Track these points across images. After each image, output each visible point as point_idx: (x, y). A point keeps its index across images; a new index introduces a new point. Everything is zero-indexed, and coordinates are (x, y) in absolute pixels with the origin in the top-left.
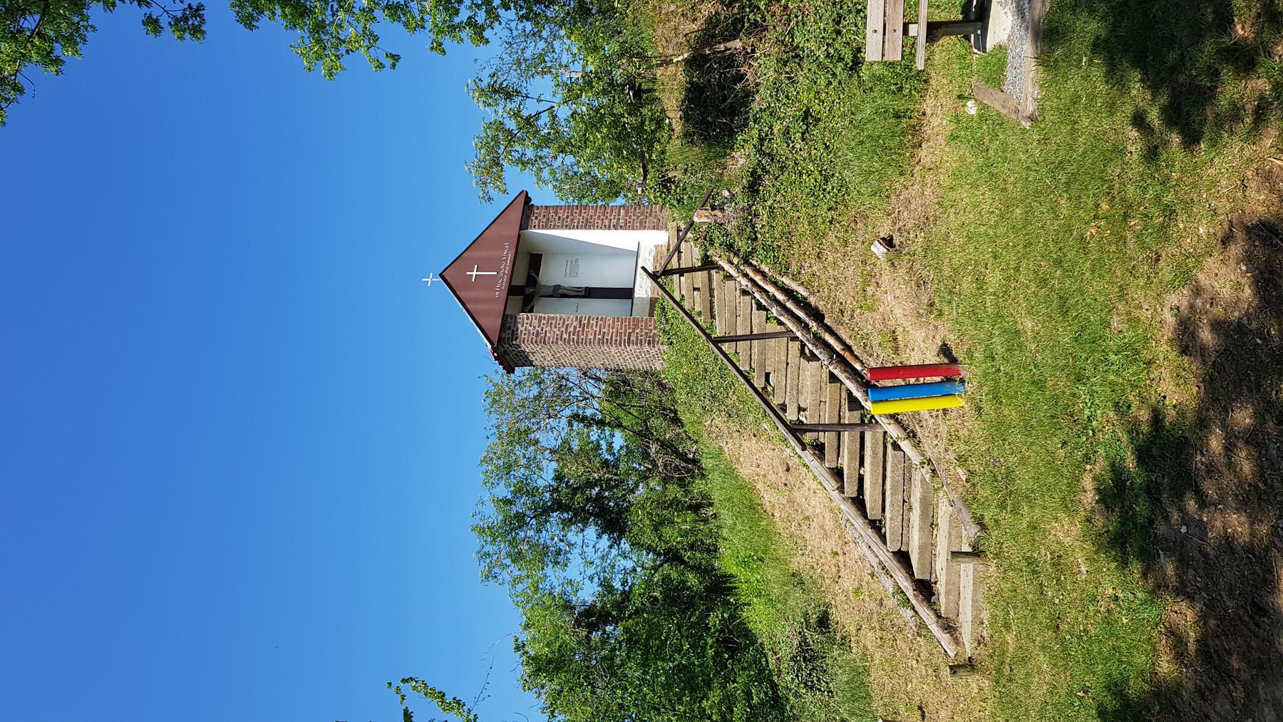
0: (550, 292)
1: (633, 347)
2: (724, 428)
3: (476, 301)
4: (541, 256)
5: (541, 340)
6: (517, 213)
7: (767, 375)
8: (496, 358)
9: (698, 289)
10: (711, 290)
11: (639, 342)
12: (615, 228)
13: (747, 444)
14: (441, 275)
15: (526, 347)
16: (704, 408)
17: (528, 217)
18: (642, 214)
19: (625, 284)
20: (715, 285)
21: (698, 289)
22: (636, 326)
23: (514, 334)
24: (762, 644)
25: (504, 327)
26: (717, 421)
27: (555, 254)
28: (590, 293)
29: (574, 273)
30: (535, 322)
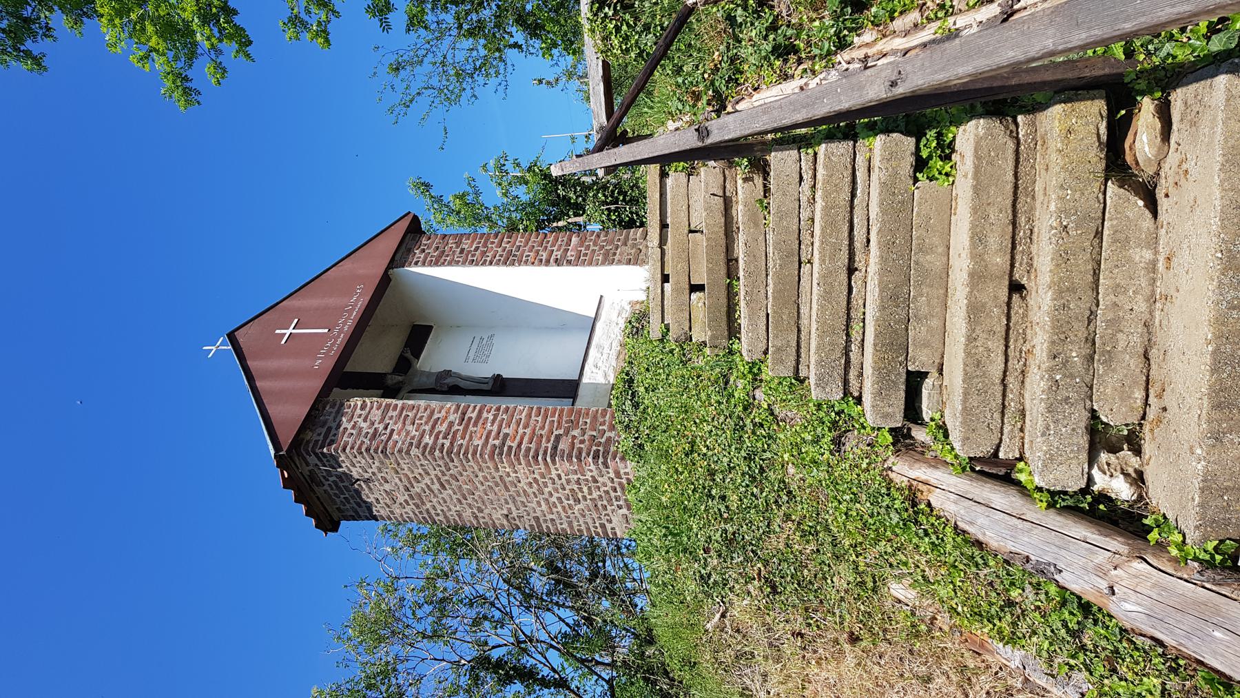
0: (430, 383)
1: (563, 467)
2: (757, 633)
5: (379, 447)
6: (389, 244)
7: (914, 382)
8: (287, 484)
9: (698, 288)
10: (731, 294)
12: (558, 262)
13: (829, 673)
14: (232, 337)
15: (353, 466)
16: (704, 579)
19: (565, 372)
20: (739, 212)
21: (698, 288)
22: (574, 424)
23: (331, 435)
25: (312, 419)
26: (740, 608)
27: (455, 327)
28: (500, 387)
29: (483, 355)
30: (376, 414)
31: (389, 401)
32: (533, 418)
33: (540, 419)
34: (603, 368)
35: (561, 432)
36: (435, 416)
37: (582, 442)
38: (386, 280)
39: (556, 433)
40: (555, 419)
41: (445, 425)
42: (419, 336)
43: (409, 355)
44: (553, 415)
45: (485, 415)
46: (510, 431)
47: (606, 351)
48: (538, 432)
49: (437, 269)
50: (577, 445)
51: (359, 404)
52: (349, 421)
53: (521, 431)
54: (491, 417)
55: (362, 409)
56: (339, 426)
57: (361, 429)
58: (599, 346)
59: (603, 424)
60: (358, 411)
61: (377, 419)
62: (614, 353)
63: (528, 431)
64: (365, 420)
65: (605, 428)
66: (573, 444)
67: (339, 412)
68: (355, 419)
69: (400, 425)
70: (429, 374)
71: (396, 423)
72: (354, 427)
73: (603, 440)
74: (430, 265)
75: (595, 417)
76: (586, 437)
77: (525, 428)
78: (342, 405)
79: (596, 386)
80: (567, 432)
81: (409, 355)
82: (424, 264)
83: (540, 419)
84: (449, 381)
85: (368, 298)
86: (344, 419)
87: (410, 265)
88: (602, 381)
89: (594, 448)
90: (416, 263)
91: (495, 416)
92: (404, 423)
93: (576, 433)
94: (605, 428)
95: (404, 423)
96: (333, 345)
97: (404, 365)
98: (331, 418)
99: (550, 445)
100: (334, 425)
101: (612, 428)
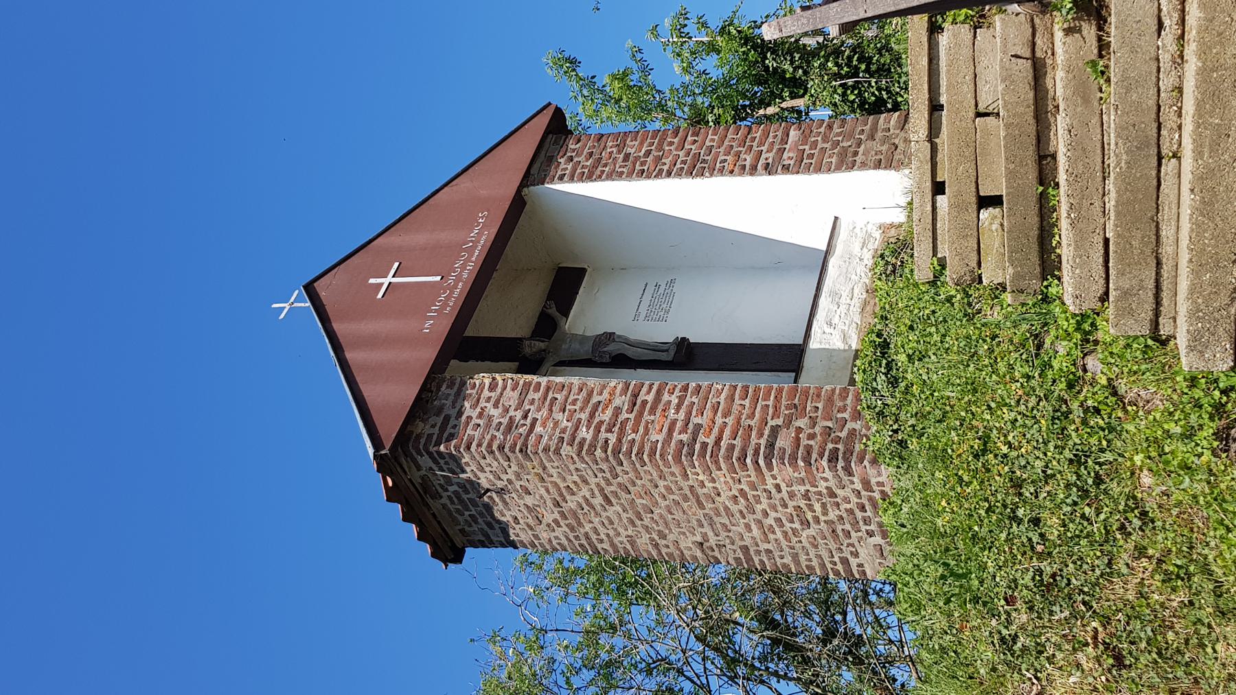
0: (585, 351)
1: (783, 473)
3: (371, 342)
4: (581, 272)
5: (517, 444)
9: (995, 201)
11: (802, 455)
12: (769, 170)
15: (481, 470)
16: (1007, 643)
17: (551, 160)
18: (851, 135)
19: (782, 332)
20: (1059, 83)
21: (995, 201)
22: (798, 410)
24: (1060, 256)
25: (422, 405)
28: (687, 356)
29: (658, 311)
30: (511, 397)
31: (529, 377)
32: (737, 401)
33: (747, 402)
34: (841, 326)
35: (780, 422)
36: (595, 399)
37: (812, 437)
38: (518, 204)
39: (771, 423)
40: (771, 403)
41: (609, 412)
42: (566, 284)
43: (553, 311)
44: (766, 398)
45: (666, 397)
46: (703, 420)
47: (845, 300)
48: (745, 422)
49: (590, 184)
50: (804, 442)
51: (487, 382)
52: (474, 407)
53: (719, 420)
54: (675, 401)
55: (492, 389)
56: (460, 414)
57: (490, 418)
58: (835, 295)
59: (843, 409)
60: (486, 393)
61: (513, 403)
62: (856, 304)
63: (730, 421)
64: (496, 406)
65: (846, 415)
66: (798, 439)
67: (460, 395)
68: (482, 404)
69: (545, 412)
70: (583, 339)
71: (539, 410)
72: (480, 415)
73: (843, 434)
74: (581, 180)
75: (830, 400)
76: (817, 430)
77: (725, 415)
78: (463, 384)
79: (830, 353)
80: (788, 422)
81: (553, 311)
82: (572, 179)
83: (747, 402)
84: (612, 348)
85: (495, 230)
86: (467, 404)
87: (552, 181)
88: (839, 345)
89: (830, 446)
90: (561, 178)
91: (681, 400)
92: (551, 410)
93: (802, 423)
94: (846, 415)
95: (551, 410)
96: (448, 298)
97: (546, 326)
98: (448, 403)
99: (763, 442)
100: (453, 412)
101: (857, 416)
